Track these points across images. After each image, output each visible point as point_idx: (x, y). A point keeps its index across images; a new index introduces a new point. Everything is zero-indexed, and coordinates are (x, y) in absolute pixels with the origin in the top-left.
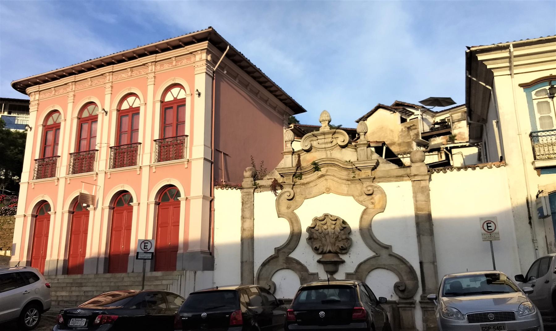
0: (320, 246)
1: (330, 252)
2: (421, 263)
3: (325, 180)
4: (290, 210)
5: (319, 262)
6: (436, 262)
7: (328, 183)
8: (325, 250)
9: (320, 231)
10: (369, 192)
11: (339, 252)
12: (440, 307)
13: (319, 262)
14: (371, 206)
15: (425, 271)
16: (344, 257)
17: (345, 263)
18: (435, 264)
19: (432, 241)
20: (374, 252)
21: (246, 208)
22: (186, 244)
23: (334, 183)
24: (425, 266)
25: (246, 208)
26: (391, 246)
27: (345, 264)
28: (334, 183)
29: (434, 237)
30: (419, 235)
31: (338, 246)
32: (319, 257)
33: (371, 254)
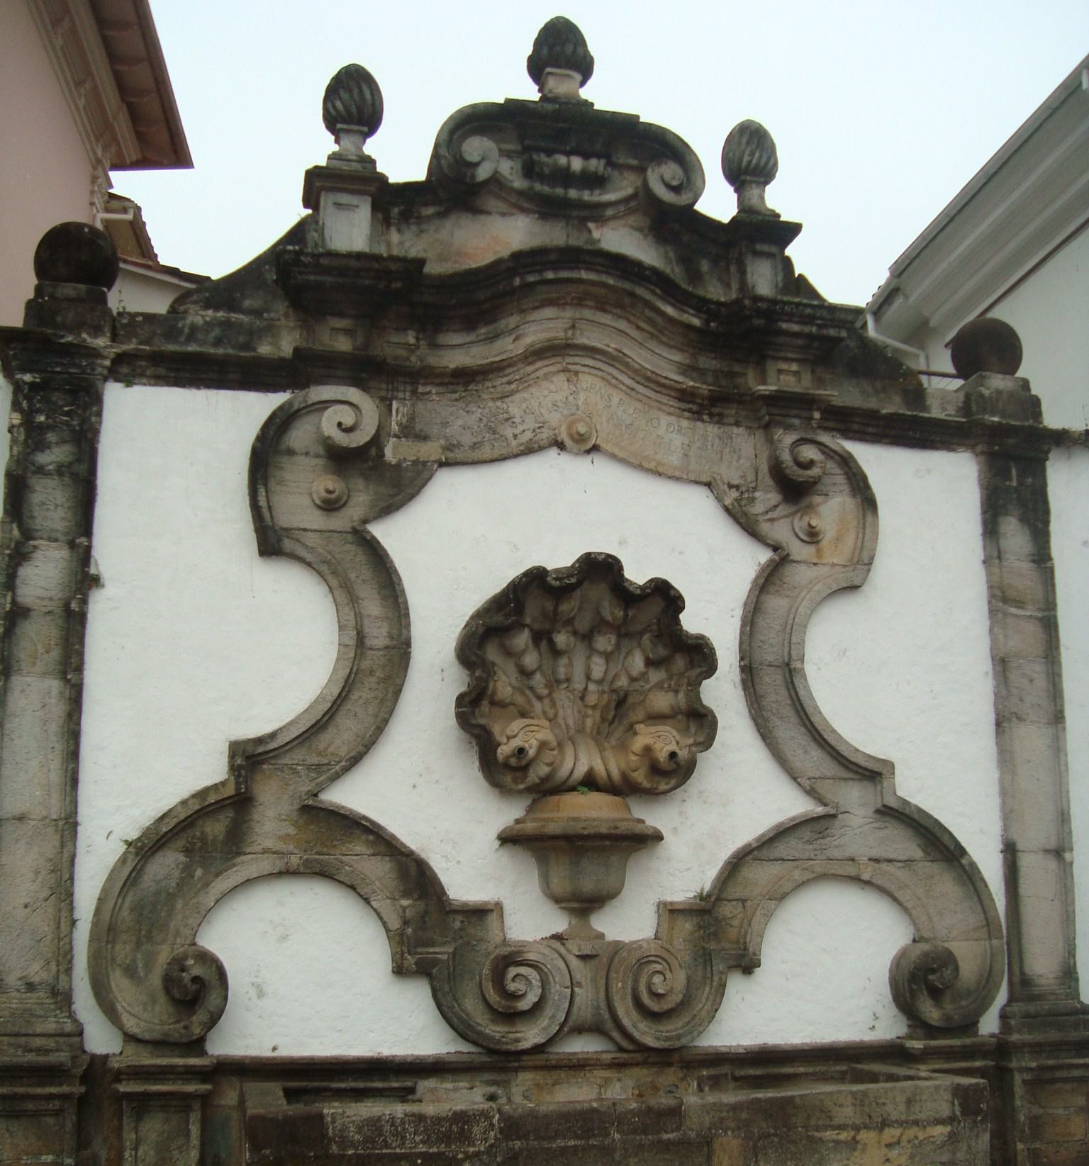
0: (543, 745)
1: (590, 783)
2: (1010, 852)
3: (562, 377)
4: (341, 521)
5: (508, 839)
6: (1071, 850)
7: (582, 396)
8: (563, 772)
9: (604, 642)
10: (801, 472)
11: (646, 784)
12: (497, 1116)
13: (508, 839)
14: (798, 550)
15: (1025, 888)
16: (654, 816)
17: (663, 841)
18: (1067, 856)
19: (1058, 748)
20: (811, 793)
21: (40, 470)
22: (46, 438)
23: (615, 400)
24: (1027, 862)
25: (40, 470)
26: (890, 765)
27: (661, 848)
28: (615, 400)
29: (1064, 729)
30: (1002, 723)
31: (648, 750)
32: (507, 814)
33: (793, 804)
